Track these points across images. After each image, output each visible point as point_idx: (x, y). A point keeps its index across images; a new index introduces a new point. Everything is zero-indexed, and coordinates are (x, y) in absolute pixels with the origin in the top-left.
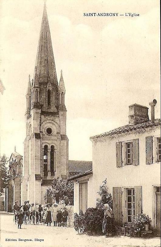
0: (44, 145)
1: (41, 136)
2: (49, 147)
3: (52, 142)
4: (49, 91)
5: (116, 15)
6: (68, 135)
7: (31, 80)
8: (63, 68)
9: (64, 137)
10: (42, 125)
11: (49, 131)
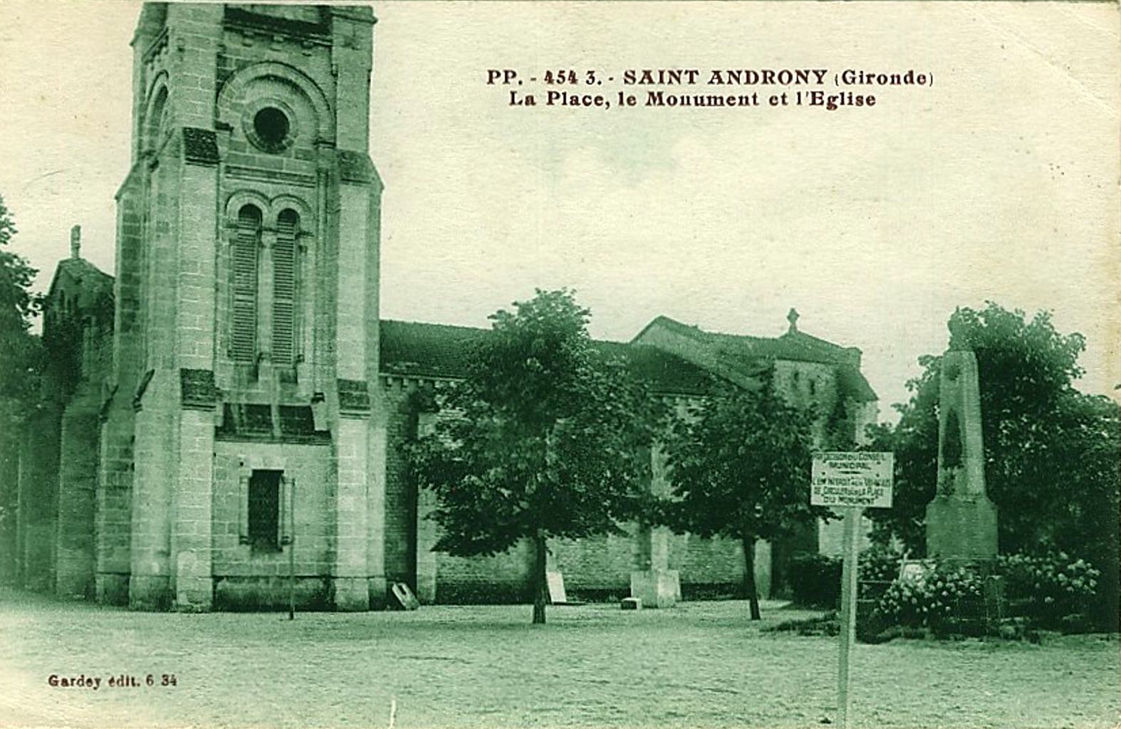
0: (236, 205)
1: (223, 149)
2: (269, 216)
6: (379, 154)
9: (351, 169)
11: (271, 128)
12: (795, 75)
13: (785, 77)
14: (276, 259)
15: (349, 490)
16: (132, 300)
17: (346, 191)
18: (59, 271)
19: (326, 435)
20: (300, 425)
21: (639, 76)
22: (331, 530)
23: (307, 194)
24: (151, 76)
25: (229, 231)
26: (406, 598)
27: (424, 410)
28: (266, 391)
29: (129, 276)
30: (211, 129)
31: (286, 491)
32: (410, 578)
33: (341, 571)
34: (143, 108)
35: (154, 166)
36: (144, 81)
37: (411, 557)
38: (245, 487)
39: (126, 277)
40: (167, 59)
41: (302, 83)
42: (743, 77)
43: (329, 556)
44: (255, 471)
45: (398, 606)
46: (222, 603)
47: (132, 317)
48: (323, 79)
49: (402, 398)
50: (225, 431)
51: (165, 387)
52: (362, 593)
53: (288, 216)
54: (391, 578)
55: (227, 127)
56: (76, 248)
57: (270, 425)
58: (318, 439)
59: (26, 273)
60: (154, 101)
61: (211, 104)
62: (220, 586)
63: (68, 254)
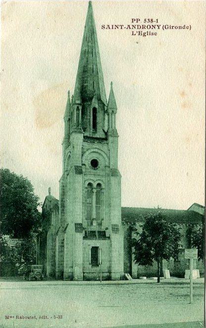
0: (87, 183)
1: (84, 170)
2: (95, 185)
3: (98, 179)
4: (95, 110)
5: (120, 27)
6: (121, 169)
7: (71, 98)
8: (115, 78)
9: (114, 173)
10: (85, 155)
11: (95, 163)
12: (151, 27)
13: (149, 27)
14: (96, 195)
15: (115, 252)
16: (63, 206)
17: (112, 178)
18: (46, 198)
19: (109, 238)
20: (103, 235)
21: (106, 27)
22: (110, 261)
23: (103, 179)
24: (67, 152)
25: (86, 189)
26: (129, 277)
27: (133, 230)
28: (95, 227)
29: (62, 200)
30: (81, 165)
31: (100, 252)
32: (130, 273)
33: (113, 271)
34: (65, 160)
35: (68, 175)
36: (65, 153)
37: (131, 267)
38: (90, 251)
39: (62, 201)
40: (70, 148)
41: (99, 151)
42: (136, 27)
43: (110, 267)
44: (92, 247)
45: (127, 279)
46: (85, 279)
47: (63, 210)
48: (106, 151)
49: (128, 227)
50: (85, 238)
51: (71, 228)
52: (118, 276)
53: (99, 185)
54: (126, 272)
55: (85, 165)
56: (50, 193)
57: (95, 236)
58: (107, 239)
59: (37, 198)
60: (68, 158)
61: (80, 159)
62: (85, 274)
63: (48, 195)
